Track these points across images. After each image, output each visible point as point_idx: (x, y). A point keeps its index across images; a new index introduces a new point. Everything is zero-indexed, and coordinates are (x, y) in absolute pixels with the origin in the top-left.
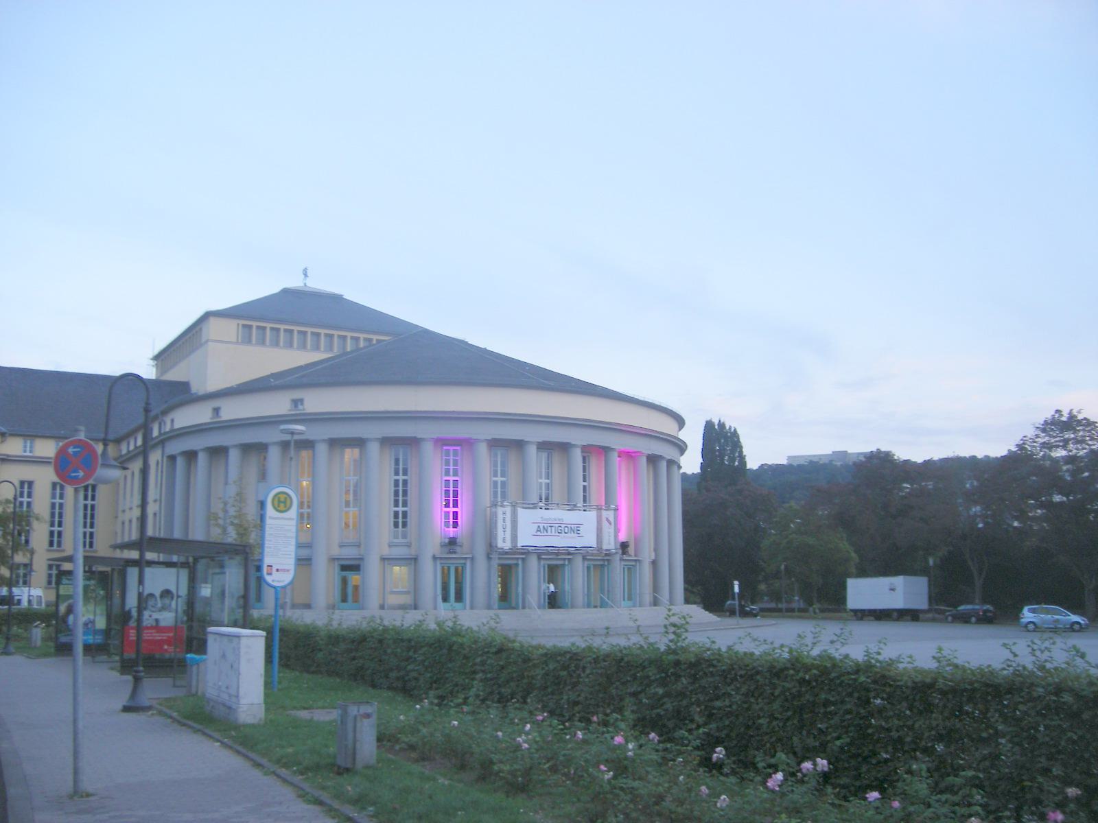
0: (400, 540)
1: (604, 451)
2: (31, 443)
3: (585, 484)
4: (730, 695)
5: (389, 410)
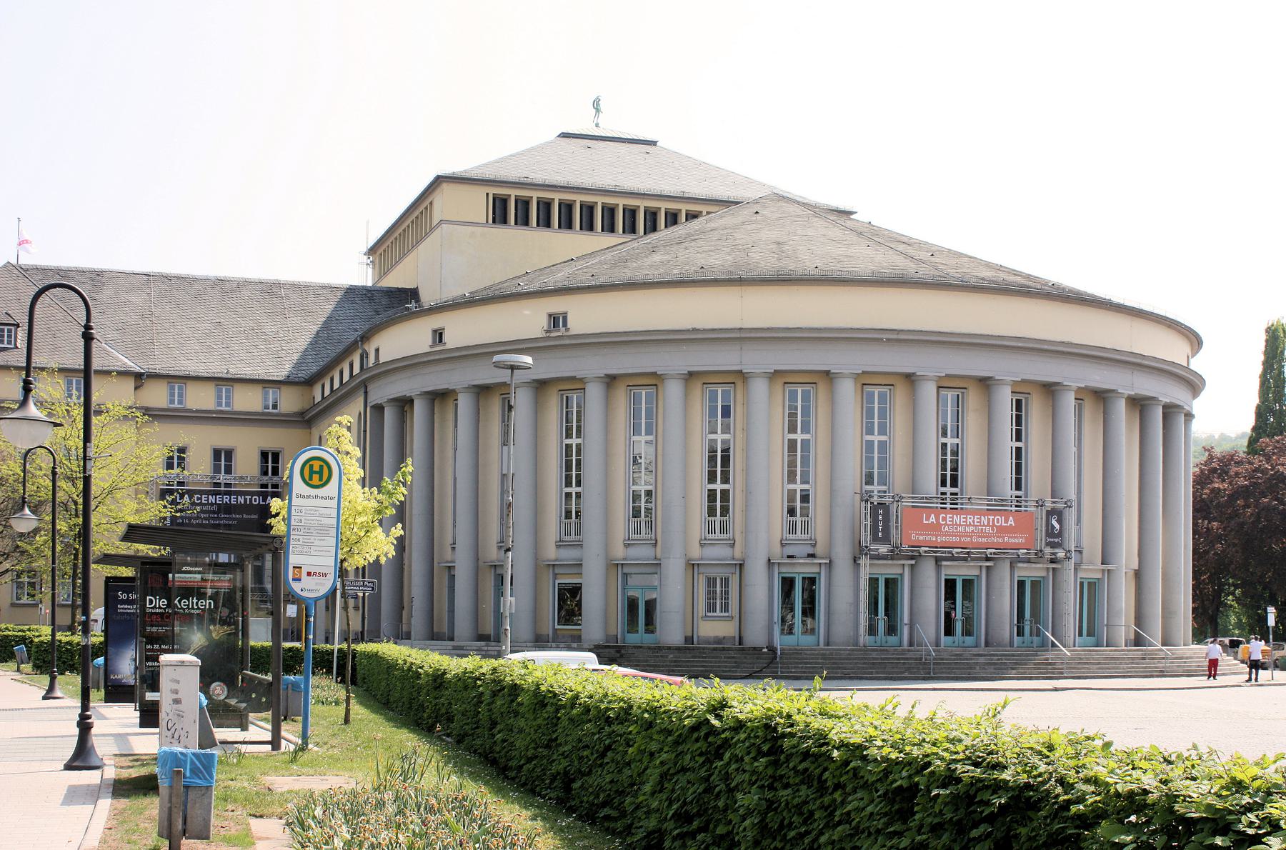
0: (718, 535)
1: (1050, 390)
2: (180, 389)
3: (1019, 444)
4: (535, 719)
5: (698, 327)
